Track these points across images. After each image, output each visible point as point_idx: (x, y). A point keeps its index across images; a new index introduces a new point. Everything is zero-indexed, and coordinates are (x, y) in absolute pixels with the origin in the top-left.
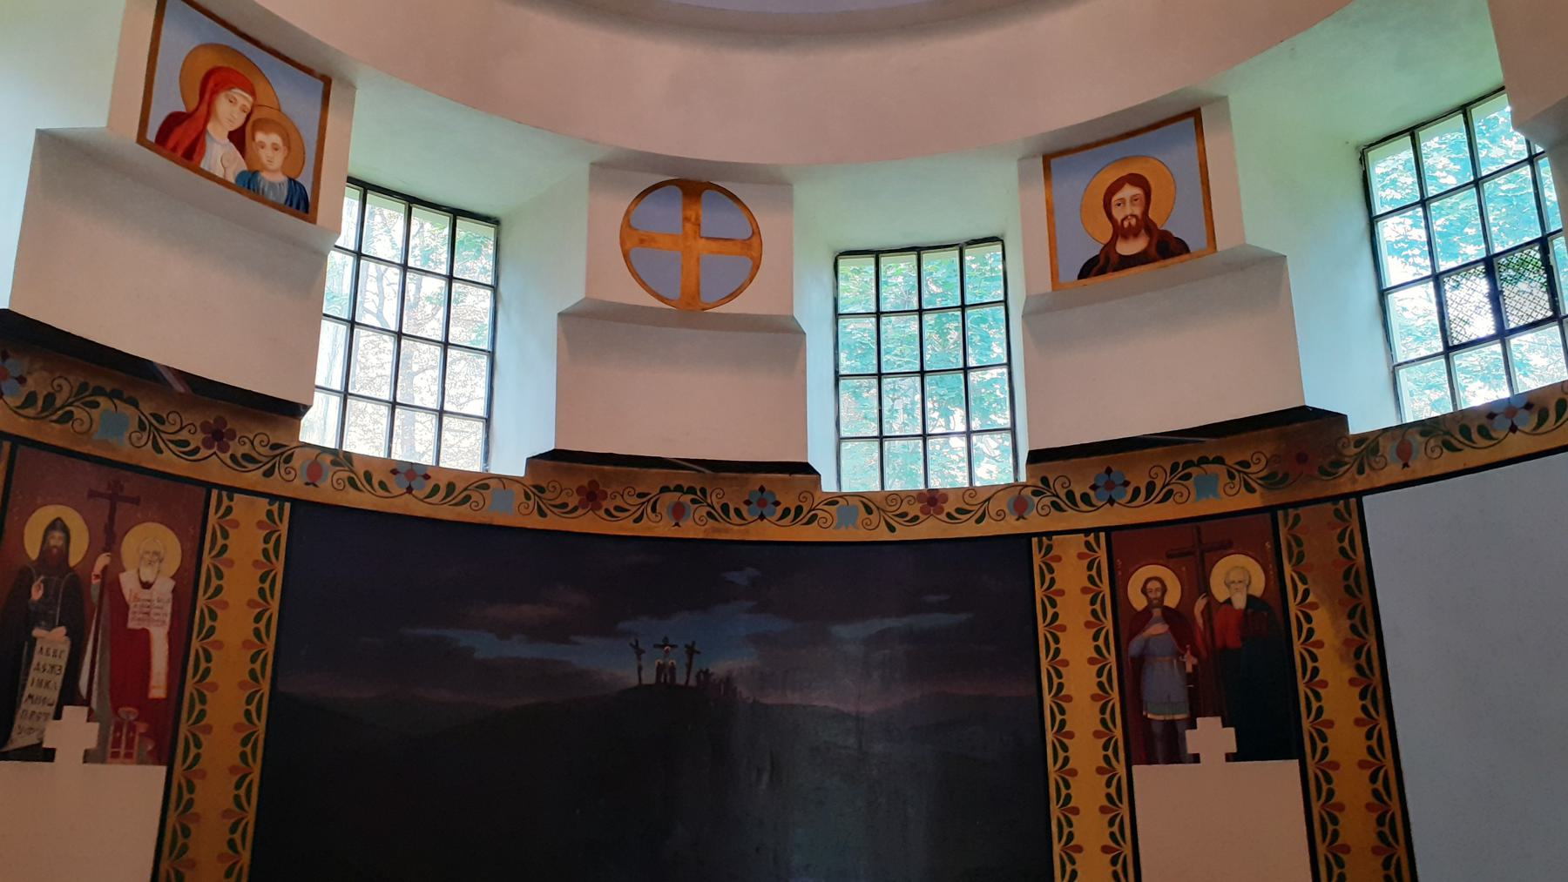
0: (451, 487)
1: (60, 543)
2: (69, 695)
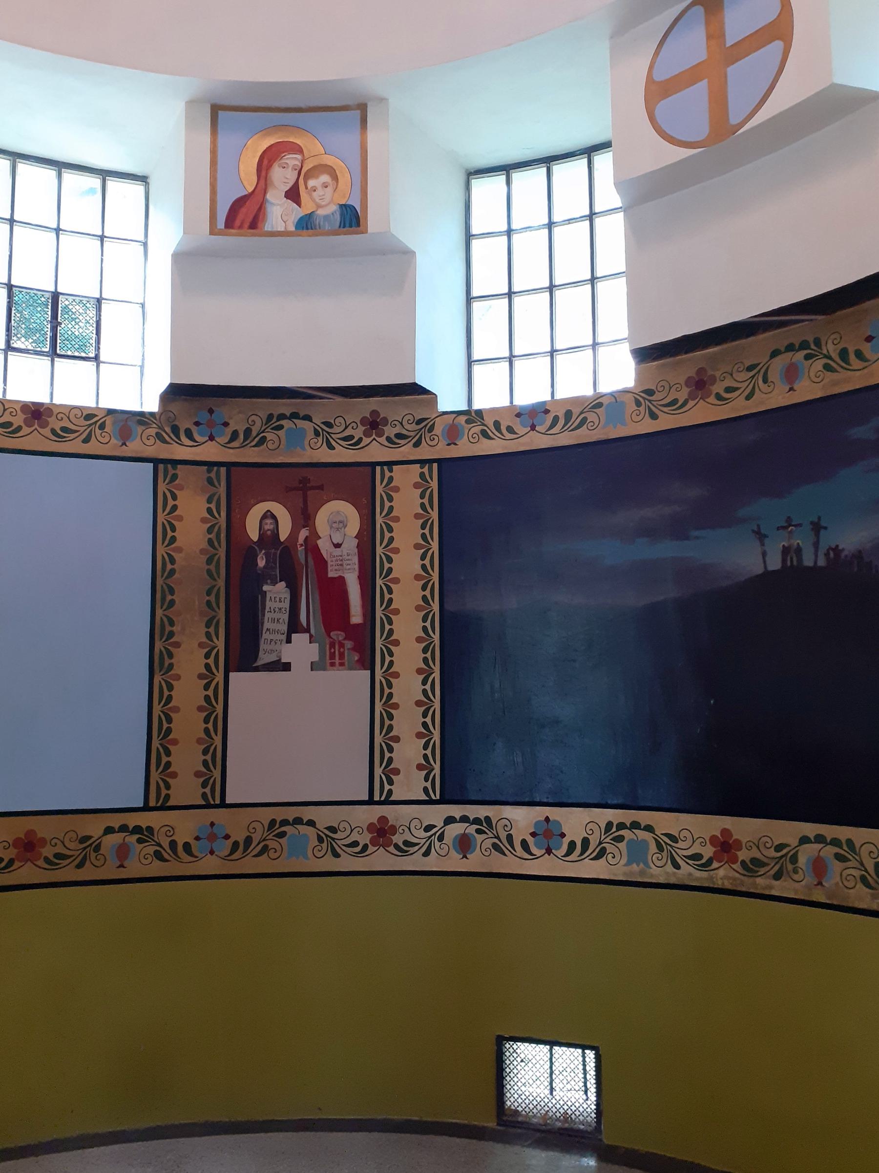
0: (568, 414)
1: (272, 527)
2: (294, 626)
